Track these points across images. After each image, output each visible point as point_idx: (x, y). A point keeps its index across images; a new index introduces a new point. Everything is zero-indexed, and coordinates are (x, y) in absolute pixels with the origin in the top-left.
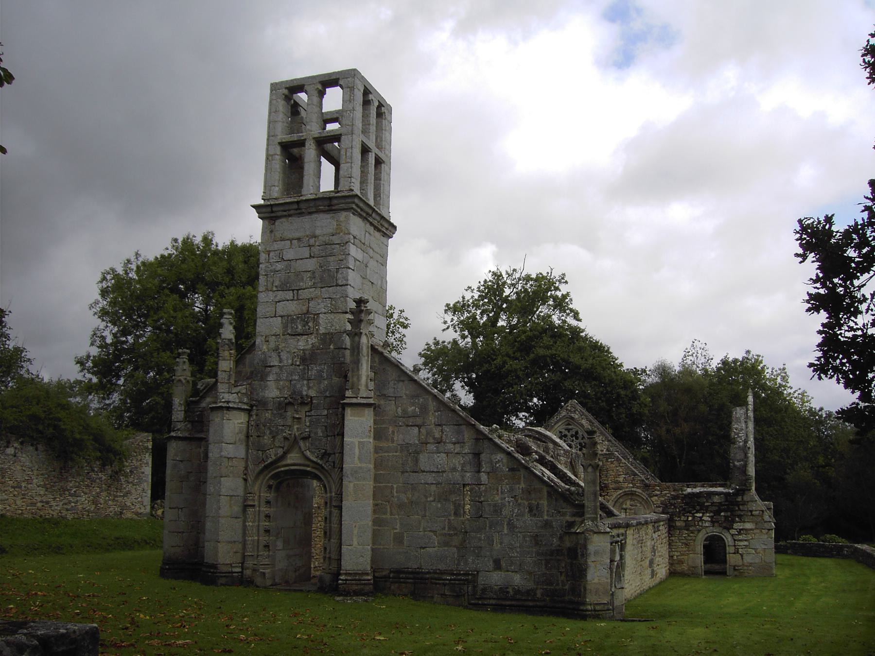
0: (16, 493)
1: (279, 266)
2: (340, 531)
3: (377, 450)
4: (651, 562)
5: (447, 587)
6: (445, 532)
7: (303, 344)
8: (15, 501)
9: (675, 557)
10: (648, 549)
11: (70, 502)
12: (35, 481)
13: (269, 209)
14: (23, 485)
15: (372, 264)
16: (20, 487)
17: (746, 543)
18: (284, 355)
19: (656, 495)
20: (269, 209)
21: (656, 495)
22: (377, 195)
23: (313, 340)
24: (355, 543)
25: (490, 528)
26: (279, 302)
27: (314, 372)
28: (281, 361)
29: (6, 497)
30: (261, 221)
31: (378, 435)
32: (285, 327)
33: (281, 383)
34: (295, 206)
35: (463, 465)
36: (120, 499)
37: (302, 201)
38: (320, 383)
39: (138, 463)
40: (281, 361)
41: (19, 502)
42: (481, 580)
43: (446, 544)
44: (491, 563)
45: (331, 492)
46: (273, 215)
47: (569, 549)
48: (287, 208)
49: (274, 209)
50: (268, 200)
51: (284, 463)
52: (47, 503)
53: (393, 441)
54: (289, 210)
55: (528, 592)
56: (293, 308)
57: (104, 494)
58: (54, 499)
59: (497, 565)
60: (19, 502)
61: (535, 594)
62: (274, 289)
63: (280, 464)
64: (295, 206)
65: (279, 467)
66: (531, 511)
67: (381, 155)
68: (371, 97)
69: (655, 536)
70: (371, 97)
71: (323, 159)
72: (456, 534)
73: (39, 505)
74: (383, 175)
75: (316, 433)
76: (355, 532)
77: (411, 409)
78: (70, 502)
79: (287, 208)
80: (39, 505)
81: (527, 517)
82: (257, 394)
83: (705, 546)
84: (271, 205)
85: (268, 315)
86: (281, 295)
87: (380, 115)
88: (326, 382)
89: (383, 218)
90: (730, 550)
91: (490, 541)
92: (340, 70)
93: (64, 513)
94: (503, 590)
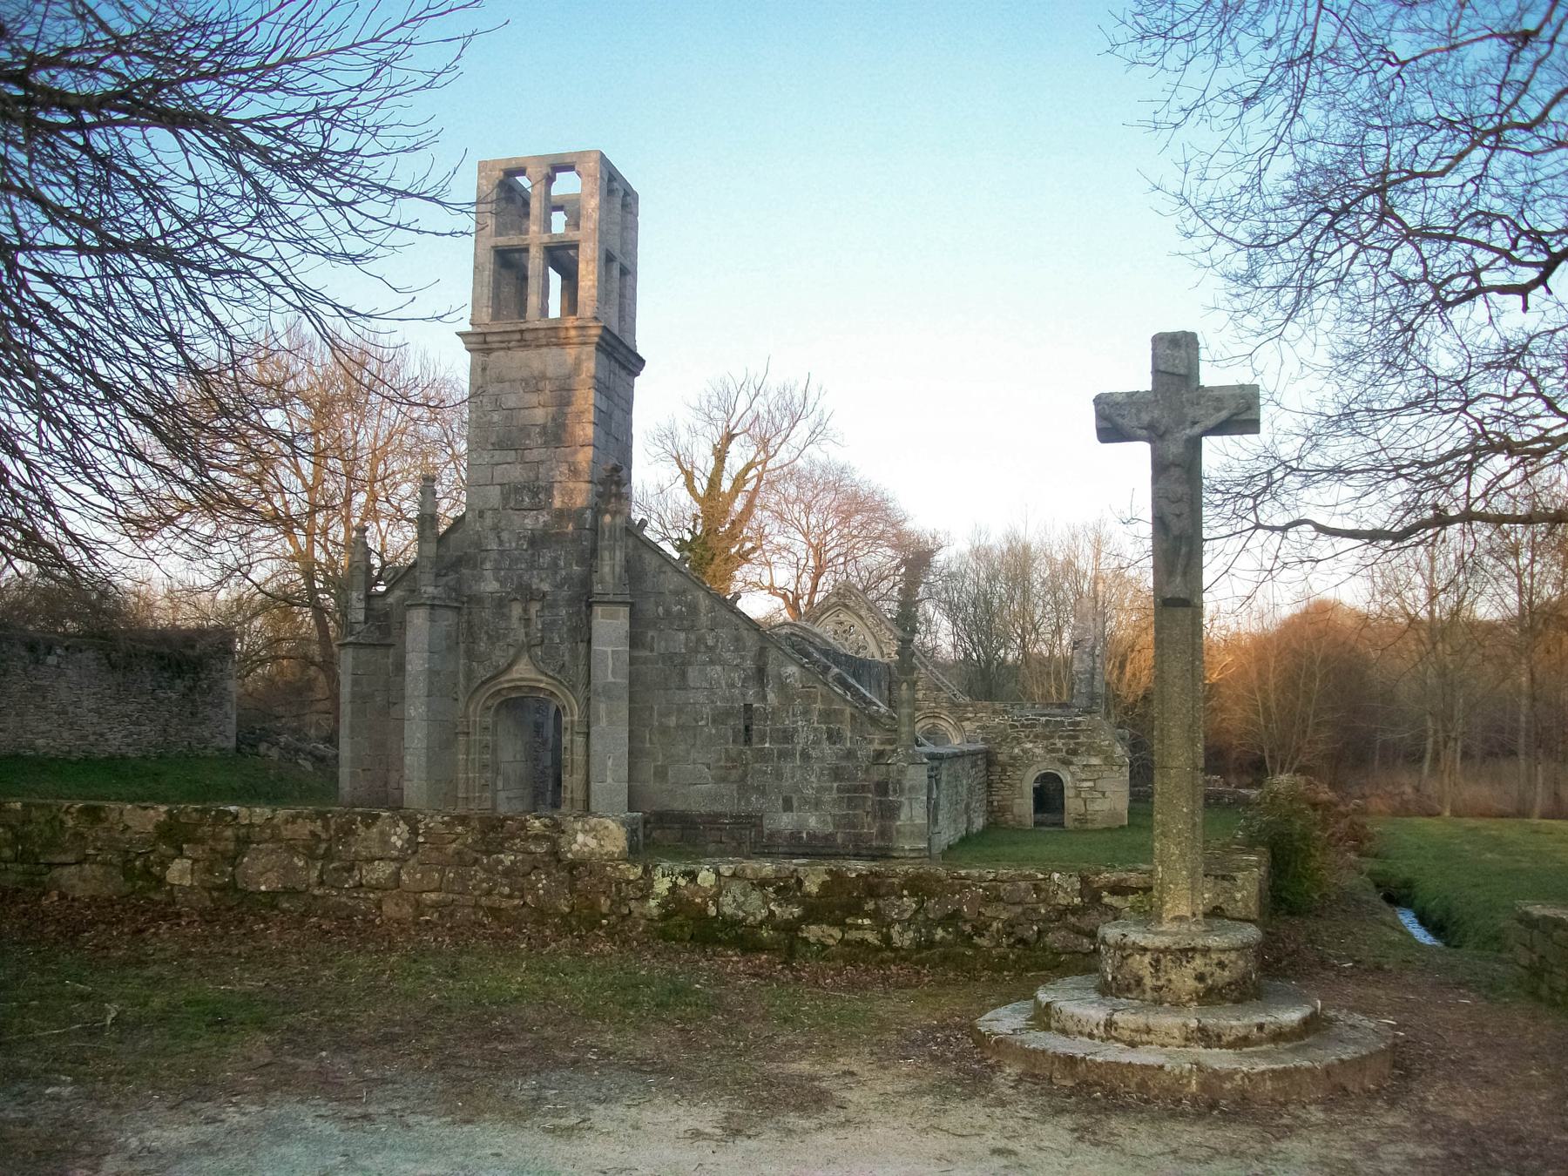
0: (61, 722)
1: (496, 417)
2: (588, 762)
3: (632, 661)
4: (968, 806)
5: (724, 833)
6: (722, 763)
7: (533, 522)
8: (60, 732)
9: (995, 804)
10: (964, 791)
11: (131, 734)
12: (85, 703)
13: (481, 339)
14: (70, 709)
15: (618, 414)
16: (66, 713)
17: (1090, 784)
18: (505, 535)
19: (969, 719)
20: (481, 339)
21: (969, 719)
22: (622, 318)
23: (544, 518)
24: (609, 780)
25: (779, 758)
26: (498, 464)
27: (548, 559)
28: (501, 542)
29: (48, 727)
30: (468, 355)
31: (635, 641)
32: (505, 498)
33: (502, 573)
34: (517, 336)
35: (744, 680)
36: (196, 729)
37: (528, 330)
38: (556, 573)
39: (218, 676)
40: (501, 542)
41: (66, 735)
42: (768, 825)
43: (724, 780)
44: (781, 801)
45: (572, 715)
46: (485, 346)
47: (878, 784)
48: (506, 337)
49: (489, 339)
50: (479, 325)
51: (507, 677)
52: (102, 735)
53: (652, 650)
54: (509, 342)
55: (827, 837)
56: (516, 473)
57: (175, 721)
58: (111, 729)
59: (788, 806)
60: (66, 735)
61: (835, 840)
62: (490, 447)
63: (502, 679)
64: (517, 336)
65: (501, 683)
66: (829, 738)
67: (627, 264)
68: (616, 185)
69: (973, 772)
70: (616, 185)
71: (551, 270)
72: (734, 767)
73: (92, 738)
74: (628, 292)
75: (551, 639)
76: (610, 763)
77: (676, 609)
78: (131, 734)
79: (506, 337)
80: (92, 738)
81: (825, 745)
82: (470, 587)
83: (1035, 789)
84: (484, 334)
85: (481, 482)
86: (498, 456)
87: (624, 206)
88: (564, 573)
89: (627, 347)
90: (1069, 793)
91: (779, 775)
92: (641, 219)
93: (124, 749)
94: (795, 836)
